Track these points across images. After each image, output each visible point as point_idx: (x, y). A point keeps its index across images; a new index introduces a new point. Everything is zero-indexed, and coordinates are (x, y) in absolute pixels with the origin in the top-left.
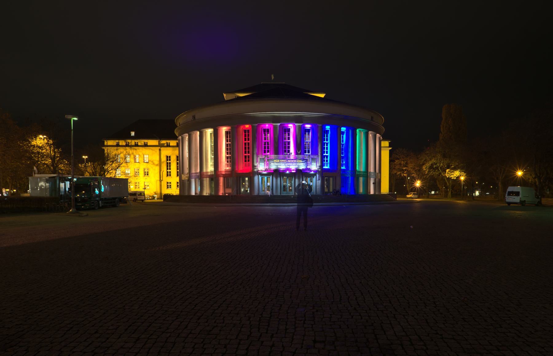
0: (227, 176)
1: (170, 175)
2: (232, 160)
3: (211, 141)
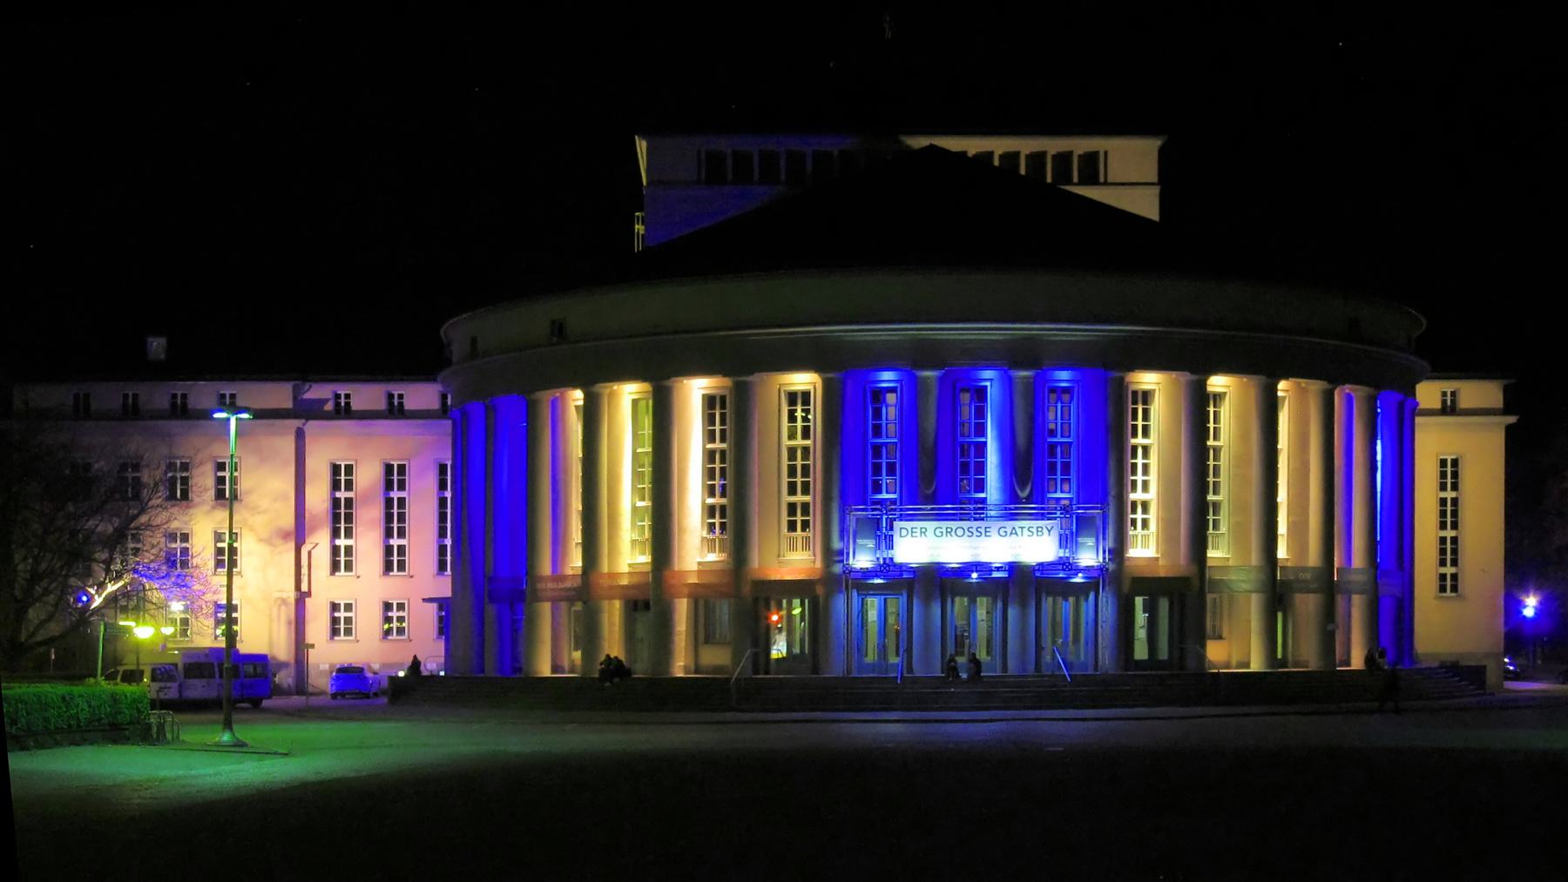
0: (703, 598)
2: (733, 522)
3: (635, 435)
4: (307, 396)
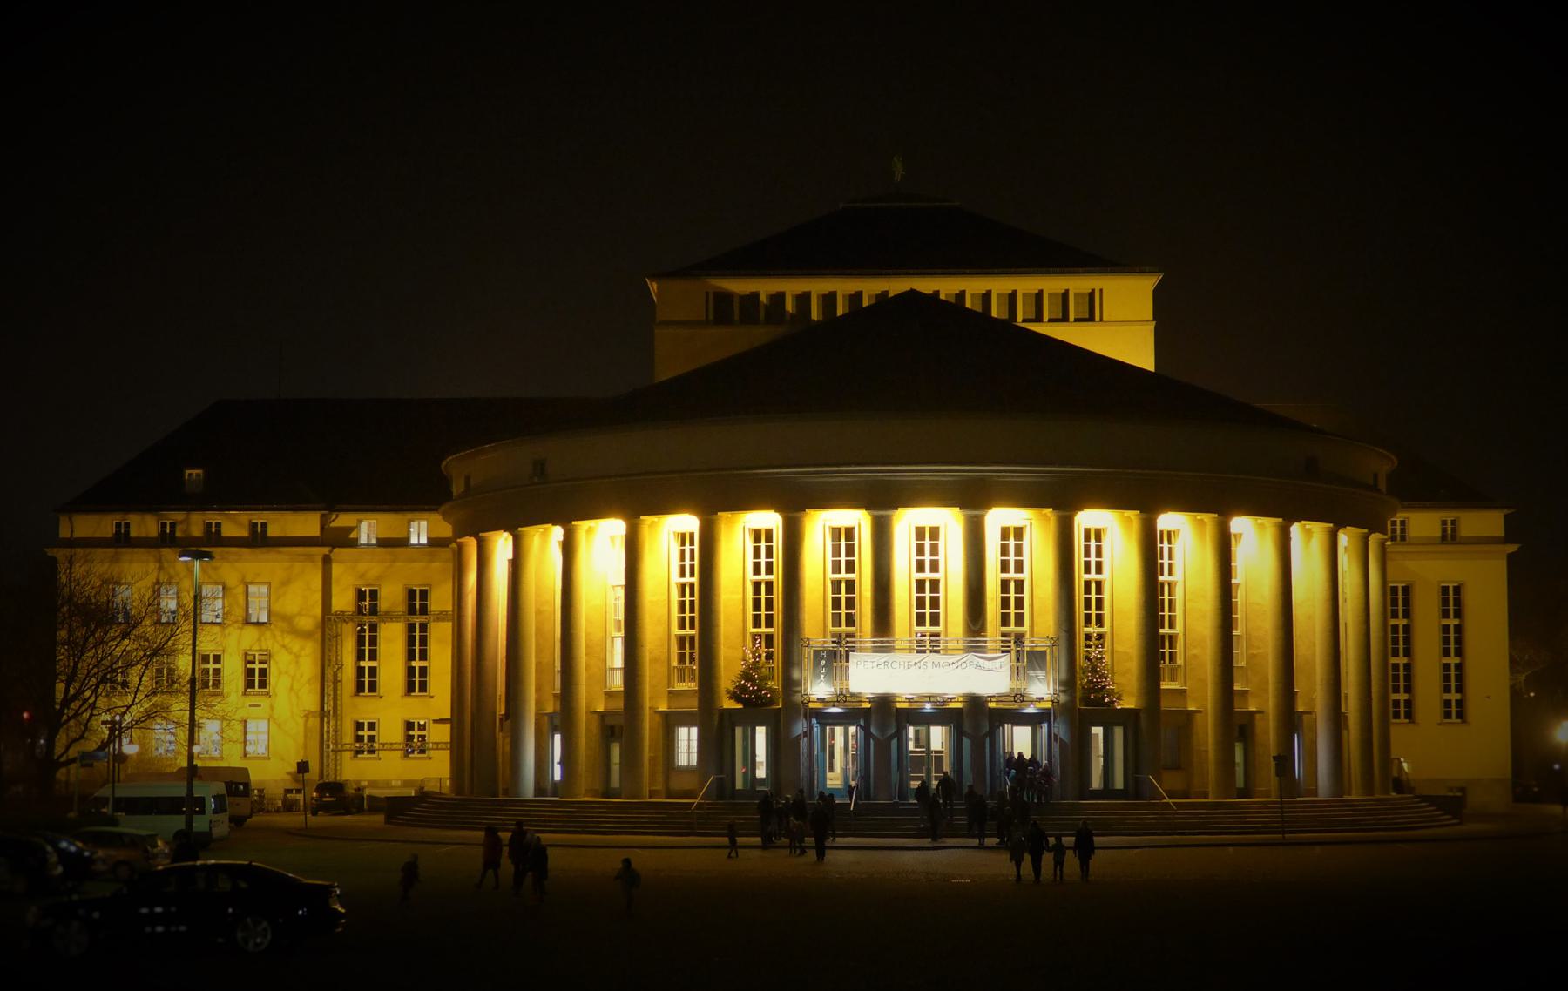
1: (423, 688)
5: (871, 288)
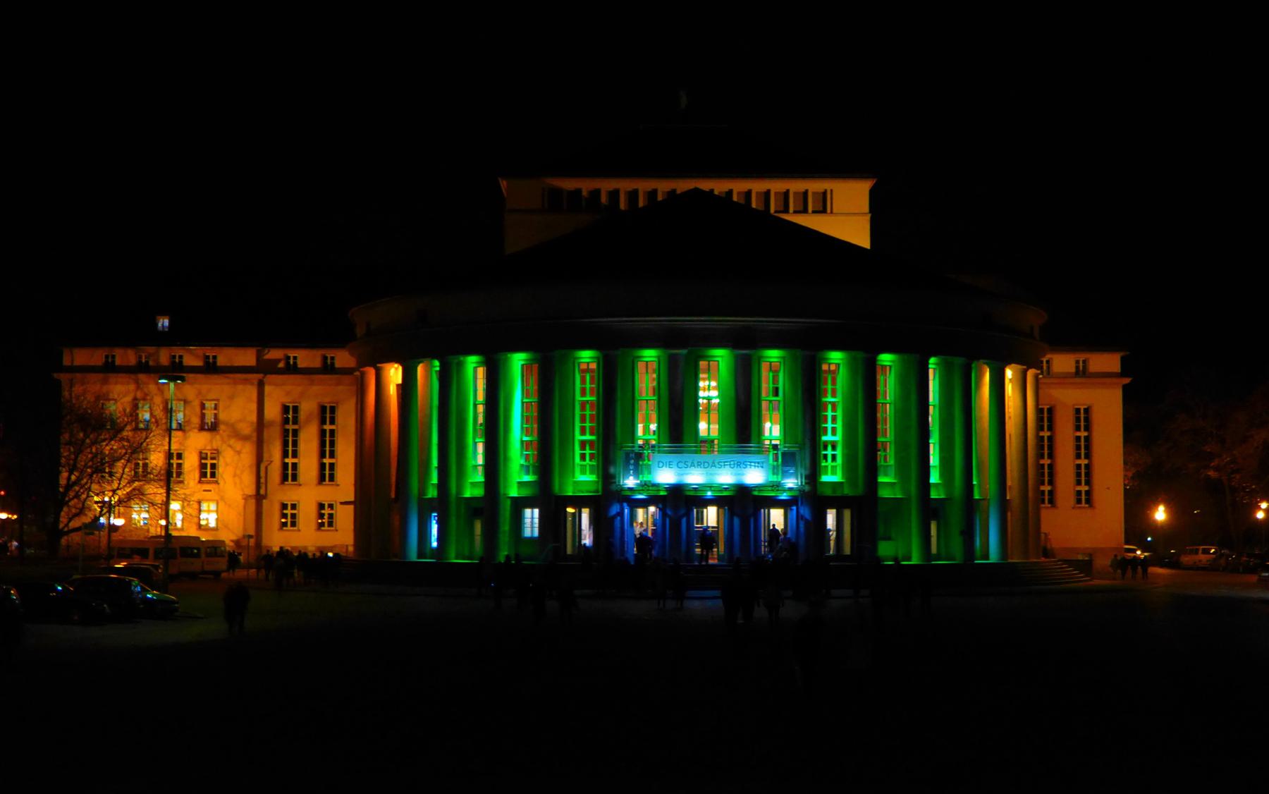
1: (332, 478)
2: (546, 455)
4: (266, 357)
5: (663, 187)
